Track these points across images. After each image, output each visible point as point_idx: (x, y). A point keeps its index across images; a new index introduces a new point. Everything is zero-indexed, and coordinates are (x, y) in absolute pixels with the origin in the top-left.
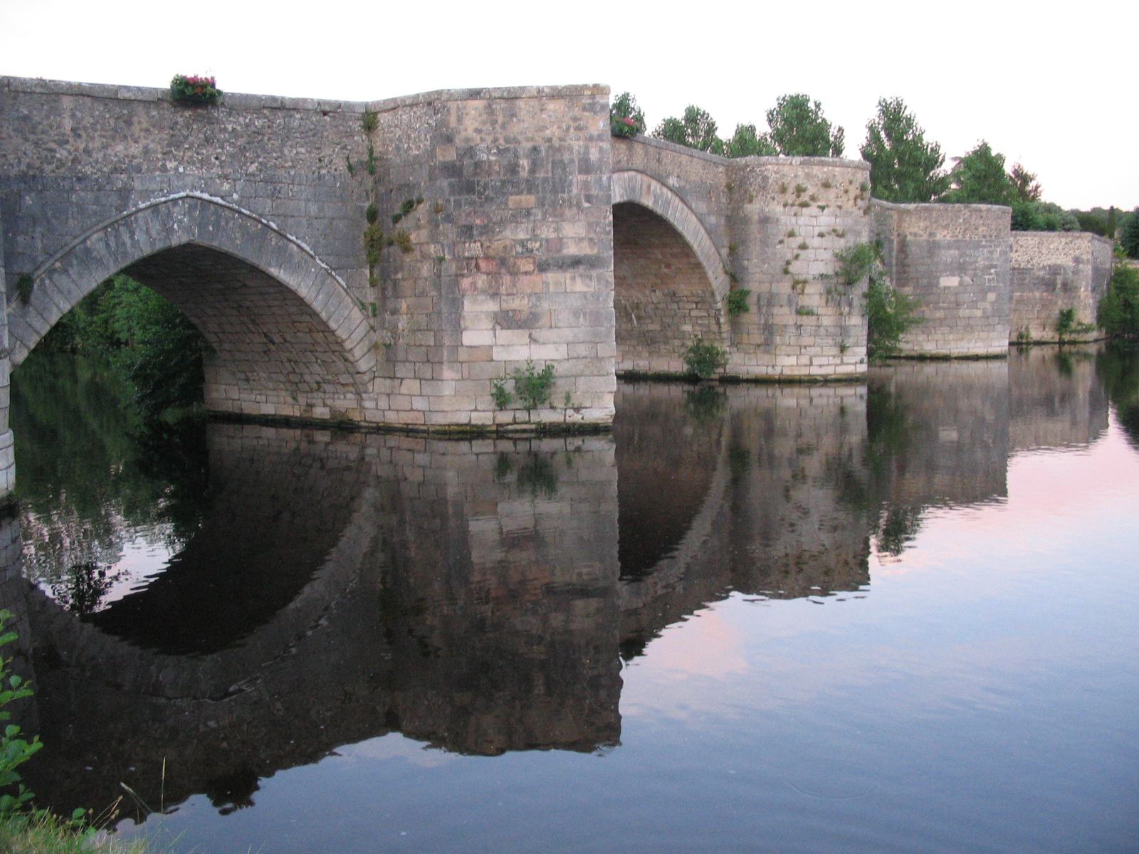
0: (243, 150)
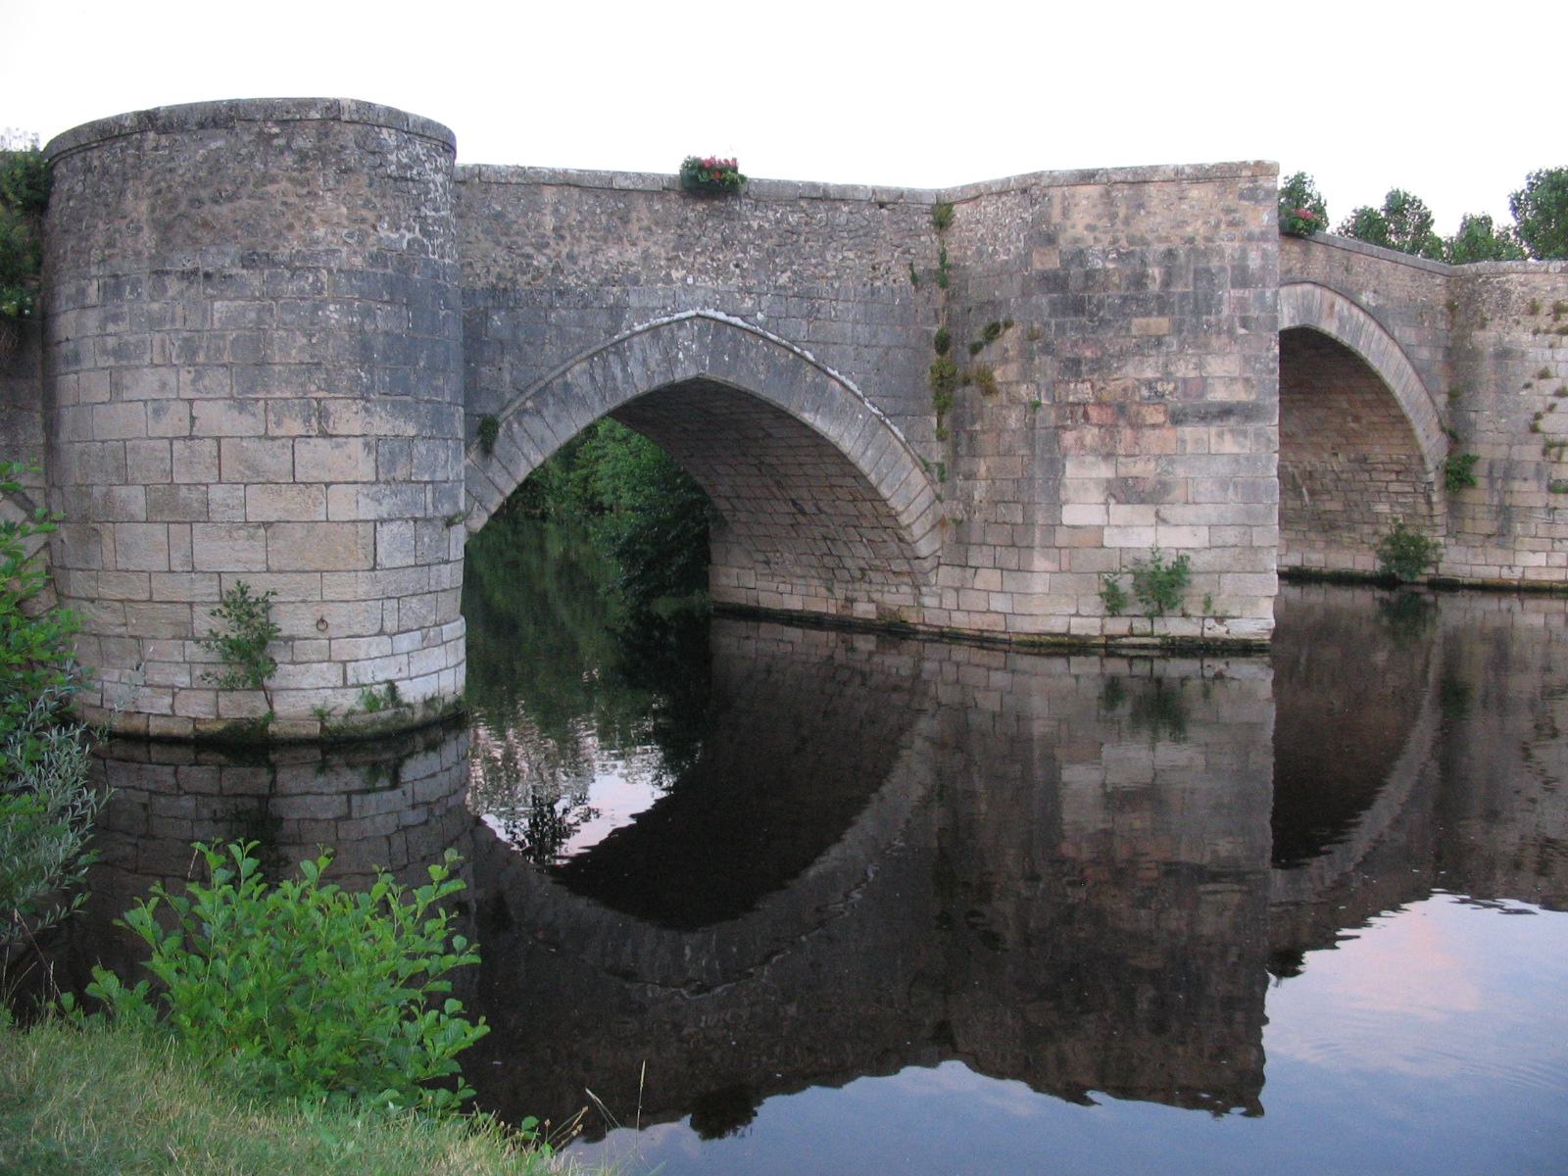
0: (771, 255)
